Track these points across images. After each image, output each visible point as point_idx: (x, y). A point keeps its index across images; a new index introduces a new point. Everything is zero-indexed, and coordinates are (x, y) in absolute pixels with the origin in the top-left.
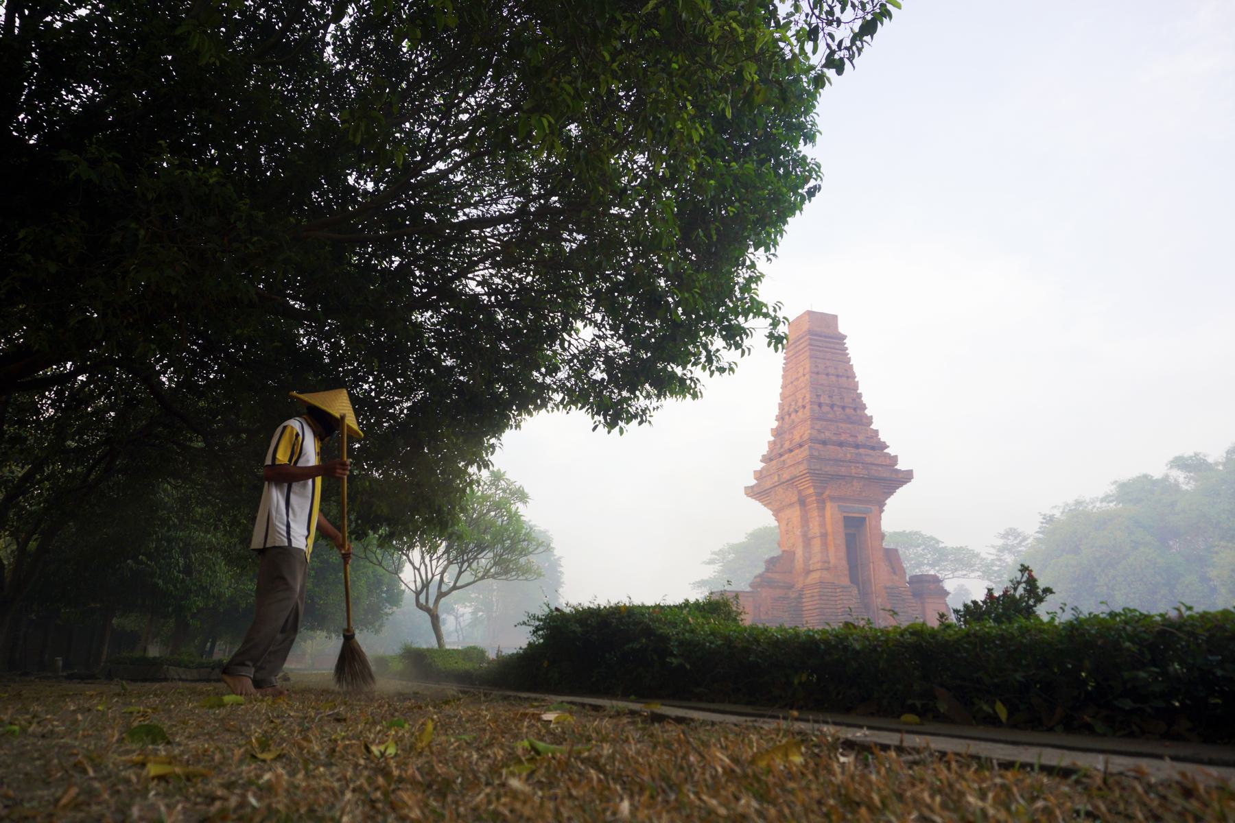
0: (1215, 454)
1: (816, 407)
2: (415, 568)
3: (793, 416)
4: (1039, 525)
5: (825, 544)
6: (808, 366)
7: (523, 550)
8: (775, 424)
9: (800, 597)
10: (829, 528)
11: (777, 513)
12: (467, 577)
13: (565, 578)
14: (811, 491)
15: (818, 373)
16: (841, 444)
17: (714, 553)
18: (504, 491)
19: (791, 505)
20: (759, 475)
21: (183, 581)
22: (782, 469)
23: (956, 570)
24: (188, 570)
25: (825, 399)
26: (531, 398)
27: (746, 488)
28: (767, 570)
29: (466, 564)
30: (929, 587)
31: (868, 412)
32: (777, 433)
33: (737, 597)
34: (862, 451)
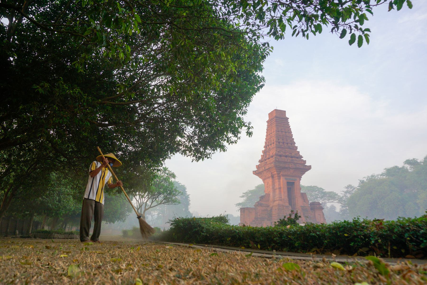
0: (420, 159)
1: (278, 143)
2: (137, 200)
3: (270, 146)
4: (359, 184)
5: (280, 192)
6: (275, 129)
7: (174, 194)
8: (264, 149)
9: (271, 210)
10: (282, 186)
11: (264, 180)
12: (155, 203)
13: (191, 202)
14: (276, 173)
15: (278, 131)
16: (286, 156)
17: (244, 193)
18: (167, 174)
19: (269, 177)
20: (258, 167)
21: (58, 205)
22: (266, 165)
23: (329, 200)
24: (59, 201)
25: (281, 140)
26: (174, 148)
27: (253, 171)
28: (260, 200)
29: (154, 199)
30: (317, 207)
31: (296, 145)
32: (264, 152)
33: (227, 215)
34: (293, 159)
